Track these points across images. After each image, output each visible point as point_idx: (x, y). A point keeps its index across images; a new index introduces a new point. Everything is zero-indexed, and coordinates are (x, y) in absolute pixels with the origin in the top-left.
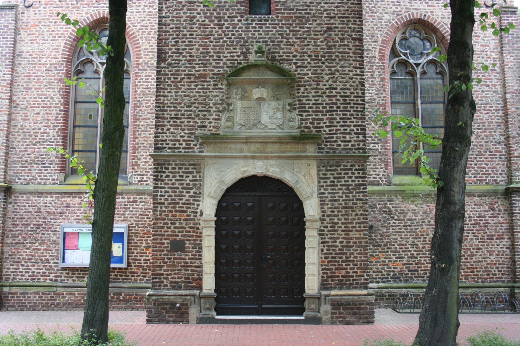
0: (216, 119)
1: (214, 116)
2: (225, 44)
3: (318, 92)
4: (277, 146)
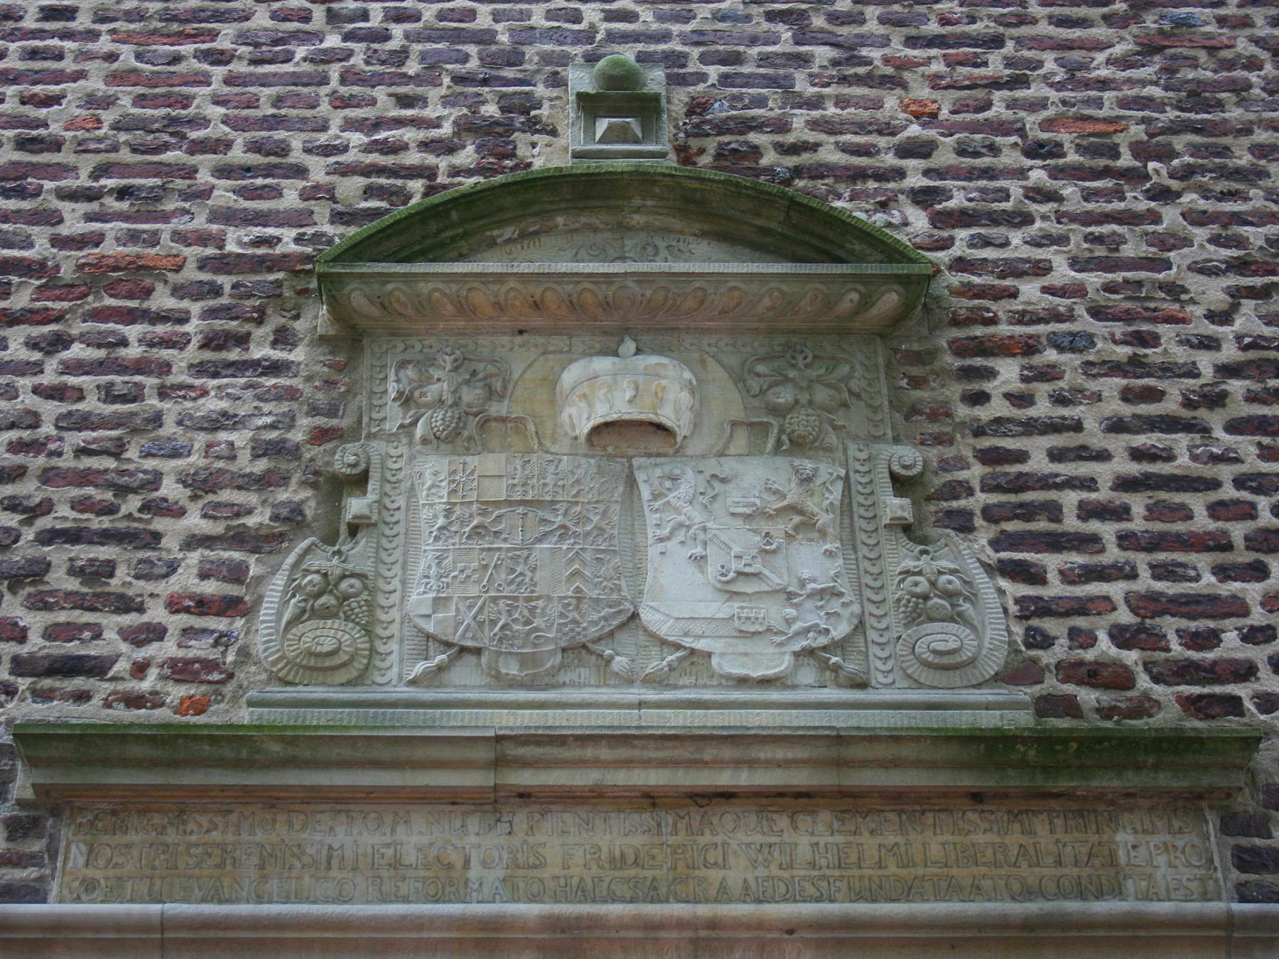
0: (202, 606)
1: (186, 580)
2: (334, 71)
3: (1154, 395)
4: (811, 838)
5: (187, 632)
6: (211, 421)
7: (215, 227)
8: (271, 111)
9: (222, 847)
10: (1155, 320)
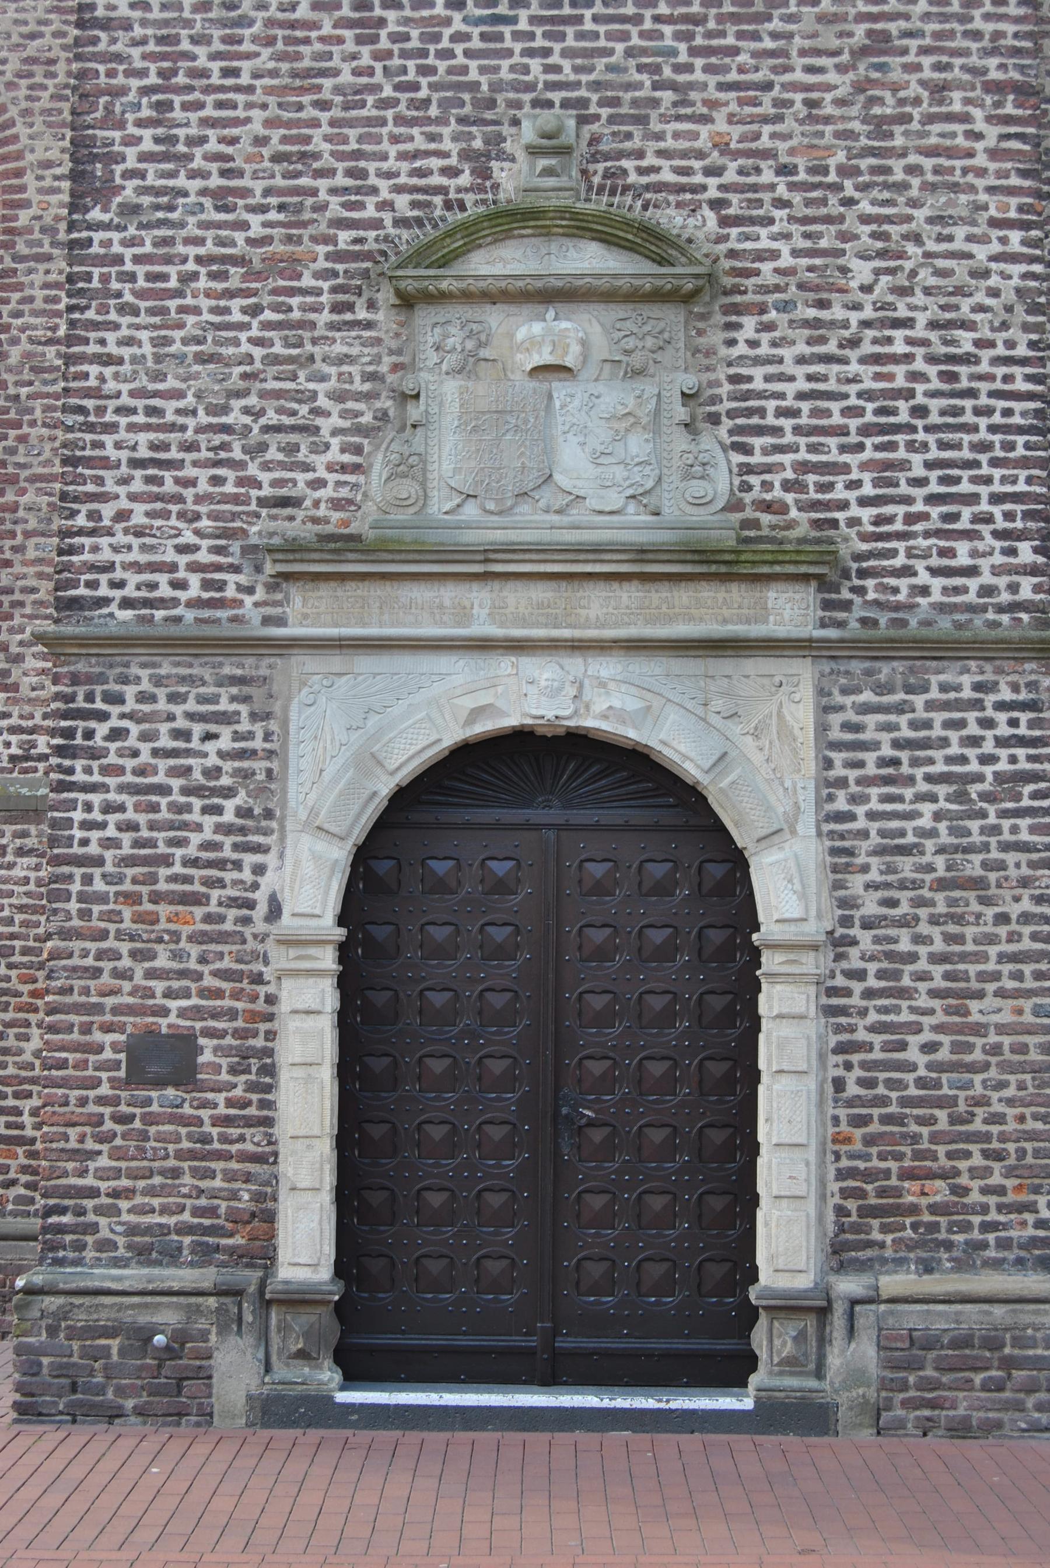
0: (344, 468)
1: (334, 454)
4: (628, 595)
5: (339, 484)
6: (341, 359)
7: (332, 231)
8: (356, 146)
9: (363, 598)
10: (831, 291)
